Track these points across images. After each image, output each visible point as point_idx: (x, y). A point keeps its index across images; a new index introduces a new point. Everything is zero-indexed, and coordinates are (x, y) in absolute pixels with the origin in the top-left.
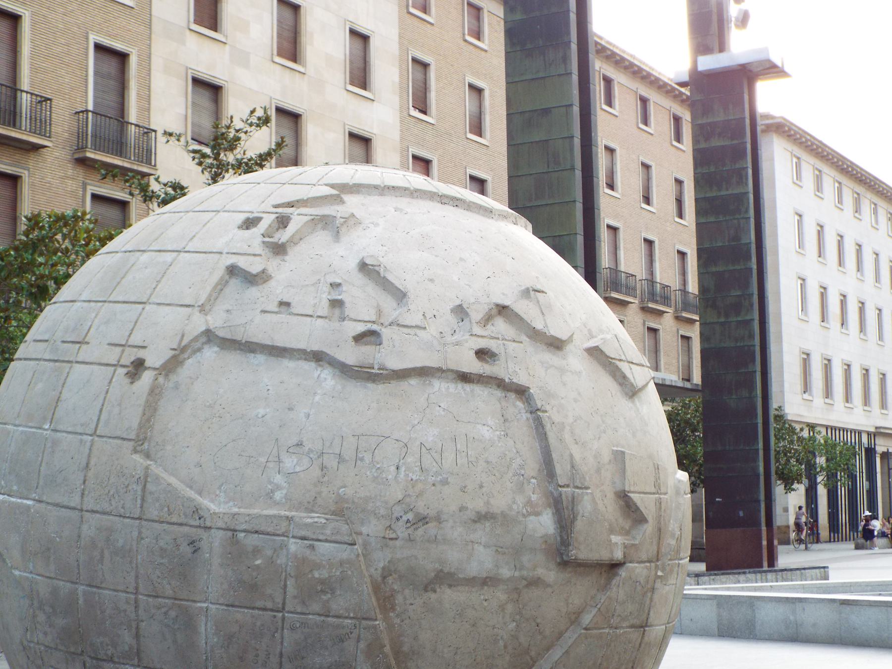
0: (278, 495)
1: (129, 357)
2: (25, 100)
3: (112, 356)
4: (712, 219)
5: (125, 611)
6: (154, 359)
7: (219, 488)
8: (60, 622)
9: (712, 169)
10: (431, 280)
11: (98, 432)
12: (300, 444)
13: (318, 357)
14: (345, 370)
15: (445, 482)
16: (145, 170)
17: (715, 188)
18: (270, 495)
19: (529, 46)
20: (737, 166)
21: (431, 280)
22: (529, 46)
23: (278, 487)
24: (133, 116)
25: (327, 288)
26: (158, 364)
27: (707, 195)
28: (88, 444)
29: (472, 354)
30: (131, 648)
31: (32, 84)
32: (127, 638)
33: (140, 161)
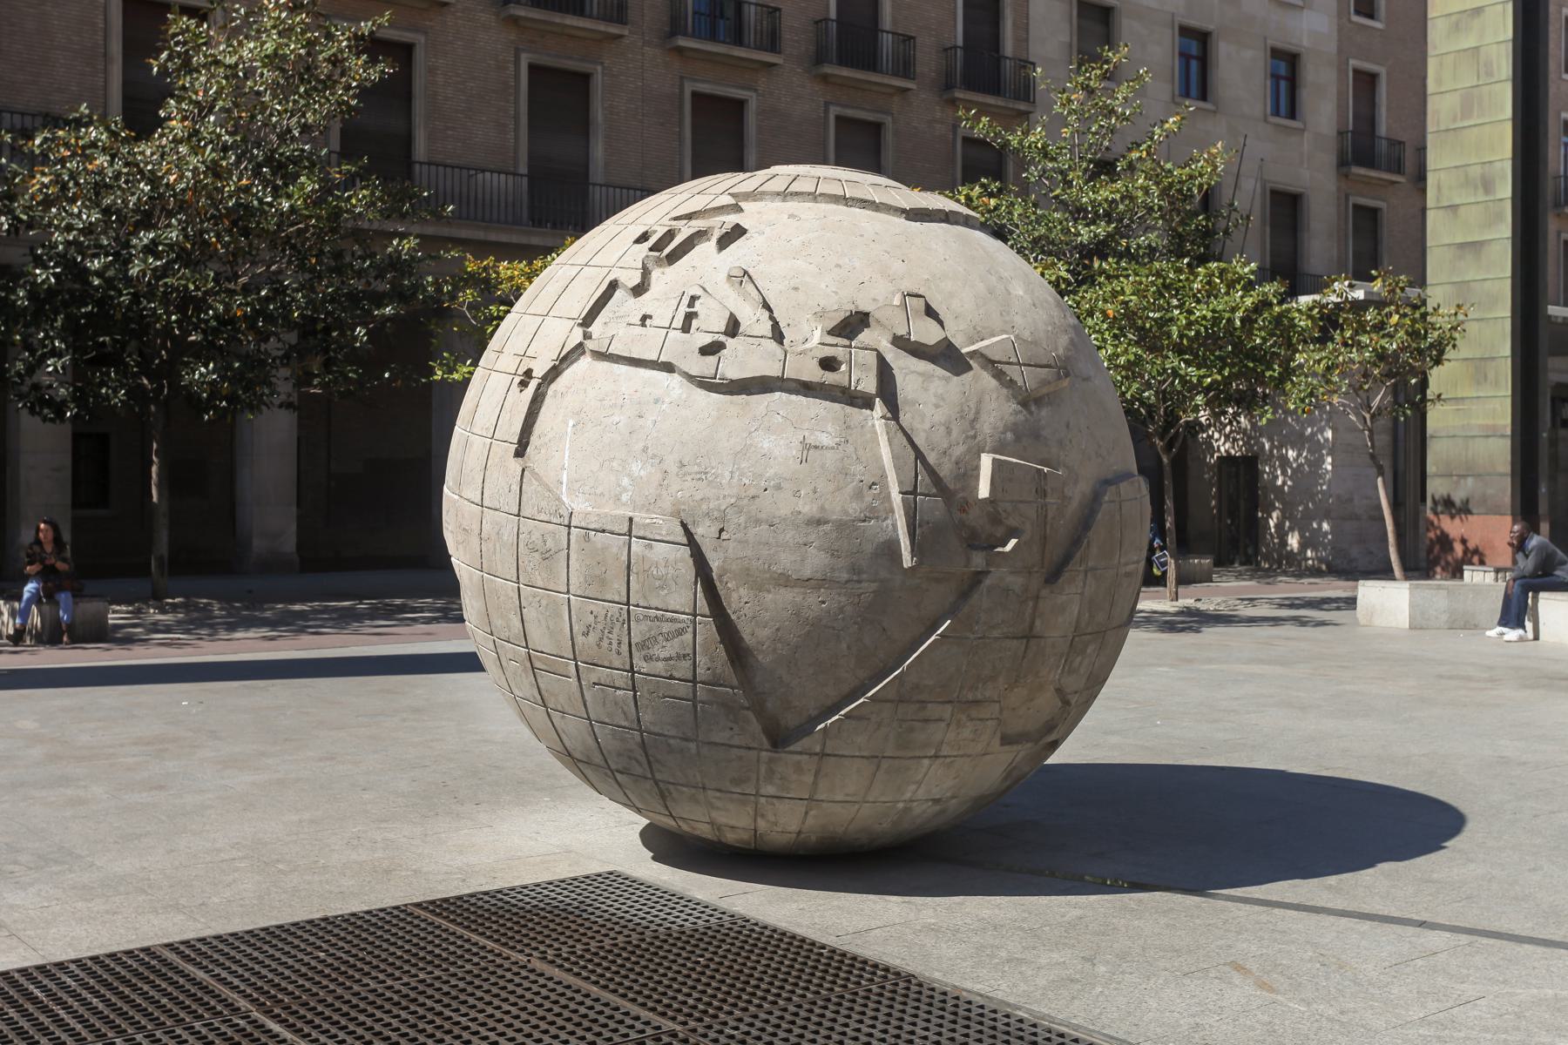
0: (624, 498)
2: (887, 41)
6: (539, 372)
10: (796, 289)
14: (691, 378)
15: (778, 487)
16: (1022, 107)
21: (796, 289)
23: (625, 490)
24: (1008, 48)
29: (815, 362)
31: (894, 21)
33: (1017, 98)
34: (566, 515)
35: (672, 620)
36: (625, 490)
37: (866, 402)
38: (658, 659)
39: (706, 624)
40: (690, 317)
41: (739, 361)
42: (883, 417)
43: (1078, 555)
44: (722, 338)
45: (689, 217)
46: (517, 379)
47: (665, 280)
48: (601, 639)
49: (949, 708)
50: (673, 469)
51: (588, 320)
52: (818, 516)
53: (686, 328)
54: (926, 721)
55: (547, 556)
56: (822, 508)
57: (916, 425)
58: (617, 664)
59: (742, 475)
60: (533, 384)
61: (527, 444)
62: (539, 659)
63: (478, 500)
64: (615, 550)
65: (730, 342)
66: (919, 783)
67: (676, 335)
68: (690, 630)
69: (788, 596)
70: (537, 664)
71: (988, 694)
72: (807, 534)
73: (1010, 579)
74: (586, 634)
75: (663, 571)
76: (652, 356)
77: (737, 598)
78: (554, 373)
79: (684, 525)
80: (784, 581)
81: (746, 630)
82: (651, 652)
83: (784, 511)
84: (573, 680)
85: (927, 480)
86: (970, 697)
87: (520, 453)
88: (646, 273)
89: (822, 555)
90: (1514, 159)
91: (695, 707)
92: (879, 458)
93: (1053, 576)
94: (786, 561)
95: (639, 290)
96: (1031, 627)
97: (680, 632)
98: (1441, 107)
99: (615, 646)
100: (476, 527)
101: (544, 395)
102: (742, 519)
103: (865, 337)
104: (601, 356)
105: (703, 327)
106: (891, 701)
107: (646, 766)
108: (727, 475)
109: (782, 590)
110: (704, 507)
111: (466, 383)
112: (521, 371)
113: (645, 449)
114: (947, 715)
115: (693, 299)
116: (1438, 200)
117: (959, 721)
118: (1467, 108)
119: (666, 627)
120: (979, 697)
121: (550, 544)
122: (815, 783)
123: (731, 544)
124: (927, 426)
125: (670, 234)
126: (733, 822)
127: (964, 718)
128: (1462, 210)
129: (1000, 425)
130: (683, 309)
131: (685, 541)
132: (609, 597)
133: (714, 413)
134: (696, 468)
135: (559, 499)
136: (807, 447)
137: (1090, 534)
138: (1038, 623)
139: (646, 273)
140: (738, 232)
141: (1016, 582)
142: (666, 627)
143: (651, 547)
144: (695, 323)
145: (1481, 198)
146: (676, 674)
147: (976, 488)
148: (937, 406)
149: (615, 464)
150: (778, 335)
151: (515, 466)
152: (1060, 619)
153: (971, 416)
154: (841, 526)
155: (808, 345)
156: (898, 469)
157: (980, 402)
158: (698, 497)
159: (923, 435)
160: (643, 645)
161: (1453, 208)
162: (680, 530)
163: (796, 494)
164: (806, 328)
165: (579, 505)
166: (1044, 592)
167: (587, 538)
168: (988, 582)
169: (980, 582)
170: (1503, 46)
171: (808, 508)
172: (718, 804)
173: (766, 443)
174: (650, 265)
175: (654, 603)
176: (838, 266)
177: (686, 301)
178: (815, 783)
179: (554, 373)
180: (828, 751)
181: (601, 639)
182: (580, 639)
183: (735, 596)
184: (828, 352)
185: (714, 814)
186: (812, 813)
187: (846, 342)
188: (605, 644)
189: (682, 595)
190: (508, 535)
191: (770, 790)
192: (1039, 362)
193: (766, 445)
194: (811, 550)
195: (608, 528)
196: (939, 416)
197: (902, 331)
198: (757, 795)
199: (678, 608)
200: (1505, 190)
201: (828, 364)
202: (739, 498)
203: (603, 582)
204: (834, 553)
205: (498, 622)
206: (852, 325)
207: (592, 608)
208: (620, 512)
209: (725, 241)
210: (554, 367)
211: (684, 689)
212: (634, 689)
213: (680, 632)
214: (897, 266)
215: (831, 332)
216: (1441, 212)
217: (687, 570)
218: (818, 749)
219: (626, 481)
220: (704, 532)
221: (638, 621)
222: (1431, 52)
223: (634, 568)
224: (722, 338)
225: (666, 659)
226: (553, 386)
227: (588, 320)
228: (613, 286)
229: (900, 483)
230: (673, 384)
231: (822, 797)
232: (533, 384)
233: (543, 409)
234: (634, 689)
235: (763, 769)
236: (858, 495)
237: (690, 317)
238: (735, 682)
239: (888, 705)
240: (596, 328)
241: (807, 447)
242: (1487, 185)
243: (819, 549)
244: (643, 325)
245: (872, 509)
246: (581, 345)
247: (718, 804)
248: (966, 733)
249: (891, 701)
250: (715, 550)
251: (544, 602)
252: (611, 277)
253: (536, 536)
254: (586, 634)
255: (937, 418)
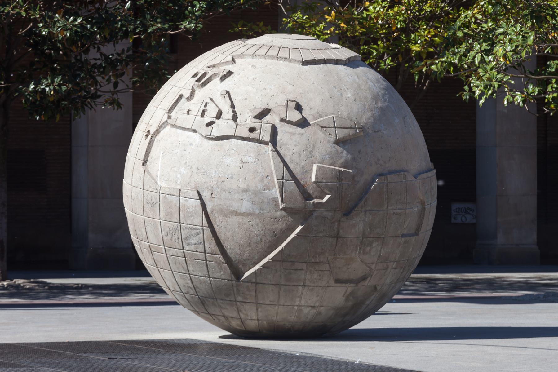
0: (179, 182)
6: (152, 132)
15: (232, 178)
21: (246, 99)
23: (179, 179)
29: (247, 129)
34: (158, 189)
35: (195, 229)
36: (179, 179)
37: (267, 143)
38: (192, 245)
39: (207, 230)
40: (204, 112)
41: (224, 127)
42: (272, 150)
43: (360, 204)
44: (214, 120)
45: (214, 66)
46: (145, 135)
47: (202, 94)
48: (172, 237)
49: (305, 265)
50: (195, 171)
51: (171, 110)
52: (246, 188)
53: (202, 116)
54: (296, 270)
55: (153, 205)
56: (248, 185)
57: (286, 153)
58: (178, 247)
59: (219, 173)
60: (150, 137)
61: (147, 160)
62: (153, 247)
63: (131, 183)
64: (175, 202)
65: (217, 121)
66: (300, 297)
67: (199, 118)
68: (202, 232)
69: (236, 219)
70: (153, 249)
71: (322, 259)
72: (243, 195)
73: (325, 213)
74: (167, 235)
75: (191, 210)
76: (189, 127)
77: (218, 221)
78: (157, 132)
79: (198, 192)
80: (235, 213)
82: (189, 241)
83: (234, 187)
84: (164, 255)
85: (288, 174)
86: (313, 260)
87: (143, 165)
88: (193, 91)
89: (249, 203)
91: (206, 262)
92: (269, 166)
93: (347, 213)
94: (235, 206)
95: (189, 99)
96: (338, 232)
97: (198, 233)
99: (177, 240)
100: (130, 194)
101: (153, 141)
102: (219, 190)
103: (268, 118)
104: (174, 126)
105: (208, 115)
106: (280, 261)
107: (194, 290)
108: (214, 173)
109: (235, 217)
110: (206, 185)
111: (169, 78)
112: (147, 131)
113: (186, 163)
114: (305, 268)
115: (206, 103)
117: (311, 270)
119: (193, 232)
120: (318, 261)
121: (154, 201)
122: (256, 296)
123: (215, 199)
124: (291, 153)
125: (204, 75)
126: (231, 315)
127: (313, 269)
129: (324, 153)
130: (203, 108)
131: (198, 198)
132: (173, 221)
133: (210, 149)
134: (203, 171)
135: (156, 183)
136: (243, 162)
137: (367, 196)
138: (341, 231)
139: (193, 91)
140: (230, 73)
141: (329, 215)
142: (193, 232)
143: (187, 200)
144: (206, 113)
146: (198, 250)
147: (311, 177)
148: (295, 146)
149: (175, 169)
150: (235, 118)
151: (142, 169)
152: (353, 231)
153: (310, 149)
154: (255, 193)
155: (246, 122)
156: (276, 170)
157: (315, 143)
158: (203, 182)
159: (289, 157)
160: (186, 239)
162: (196, 194)
163: (239, 180)
164: (247, 115)
165: (162, 184)
166: (342, 219)
167: (165, 198)
168: (315, 214)
169: (312, 214)
171: (243, 186)
172: (223, 306)
173: (228, 161)
174: (195, 88)
175: (189, 222)
176: (265, 89)
177: (204, 105)
178: (256, 296)
179: (157, 132)
180: (258, 281)
181: (172, 237)
182: (165, 238)
183: (217, 219)
184: (253, 125)
185: (223, 311)
186: (259, 310)
187: (260, 121)
188: (173, 239)
189: (198, 219)
190: (140, 198)
191: (240, 298)
192: (345, 126)
193: (228, 161)
194: (245, 202)
195: (172, 194)
196: (296, 149)
197: (283, 116)
198: (236, 301)
199: (197, 224)
201: (252, 130)
202: (218, 182)
203: (171, 215)
204: (253, 203)
205: (139, 233)
206: (263, 114)
207: (168, 225)
208: (177, 187)
209: (224, 78)
210: (157, 130)
211: (202, 256)
212: (185, 257)
213: (198, 233)
214: (290, 88)
215: (256, 117)
217: (200, 209)
218: (254, 280)
220: (206, 195)
221: (184, 229)
223: (181, 209)
224: (214, 120)
225: (195, 244)
226: (157, 137)
227: (171, 110)
228: (181, 97)
229: (277, 176)
230: (196, 137)
231: (261, 302)
232: (150, 137)
233: (153, 147)
234: (185, 257)
235: (235, 289)
236: (262, 180)
237: (204, 112)
238: (219, 253)
239: (278, 262)
240: (173, 114)
241: (243, 162)
243: (248, 201)
244: (188, 114)
245: (266, 185)
246: (166, 121)
247: (223, 306)
248: (316, 276)
249: (280, 261)
250: (210, 202)
251: (152, 223)
252: (180, 93)
253: (149, 197)
254: (167, 235)
255: (295, 151)
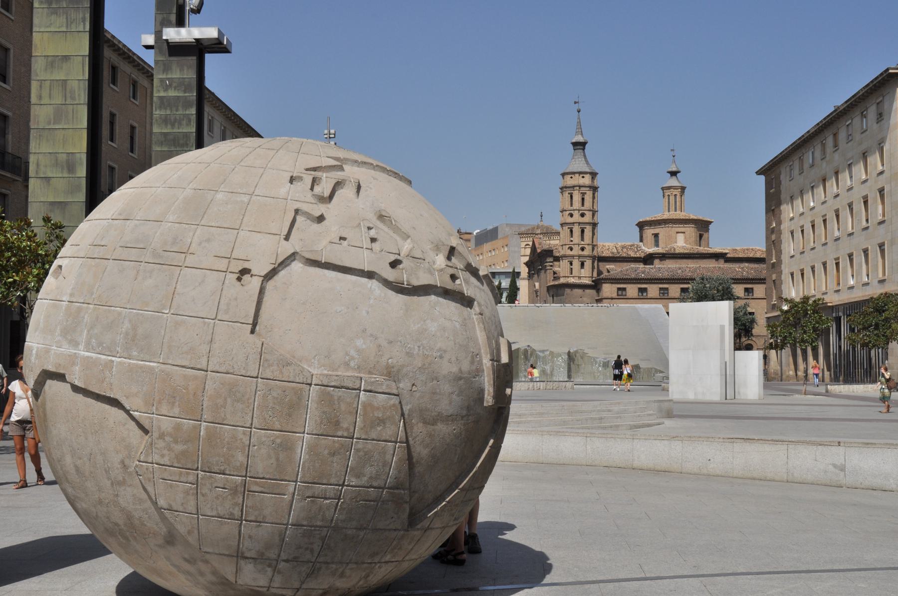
0: (352, 364)
1: (237, 267)
3: (222, 264)
4: (166, 149)
5: (241, 439)
7: (314, 358)
8: (179, 448)
9: (168, 112)
11: (219, 318)
12: (364, 331)
13: (370, 275)
14: (387, 283)
17: (169, 126)
18: (347, 364)
19: (54, 6)
20: (187, 112)
22: (54, 6)
23: (353, 358)
25: (364, 230)
26: (263, 274)
27: (163, 131)
28: (212, 325)
30: (241, 465)
32: (240, 458)
81: (415, 455)
90: (87, 153)
98: (41, 114)
116: (37, 172)
118: (59, 114)
128: (53, 181)
145: (66, 175)
161: (47, 179)
170: (82, 83)
179: (273, 273)
183: (415, 428)
200: (82, 171)
216: (39, 181)
219: (353, 353)
222: (33, 77)
242: (71, 167)
